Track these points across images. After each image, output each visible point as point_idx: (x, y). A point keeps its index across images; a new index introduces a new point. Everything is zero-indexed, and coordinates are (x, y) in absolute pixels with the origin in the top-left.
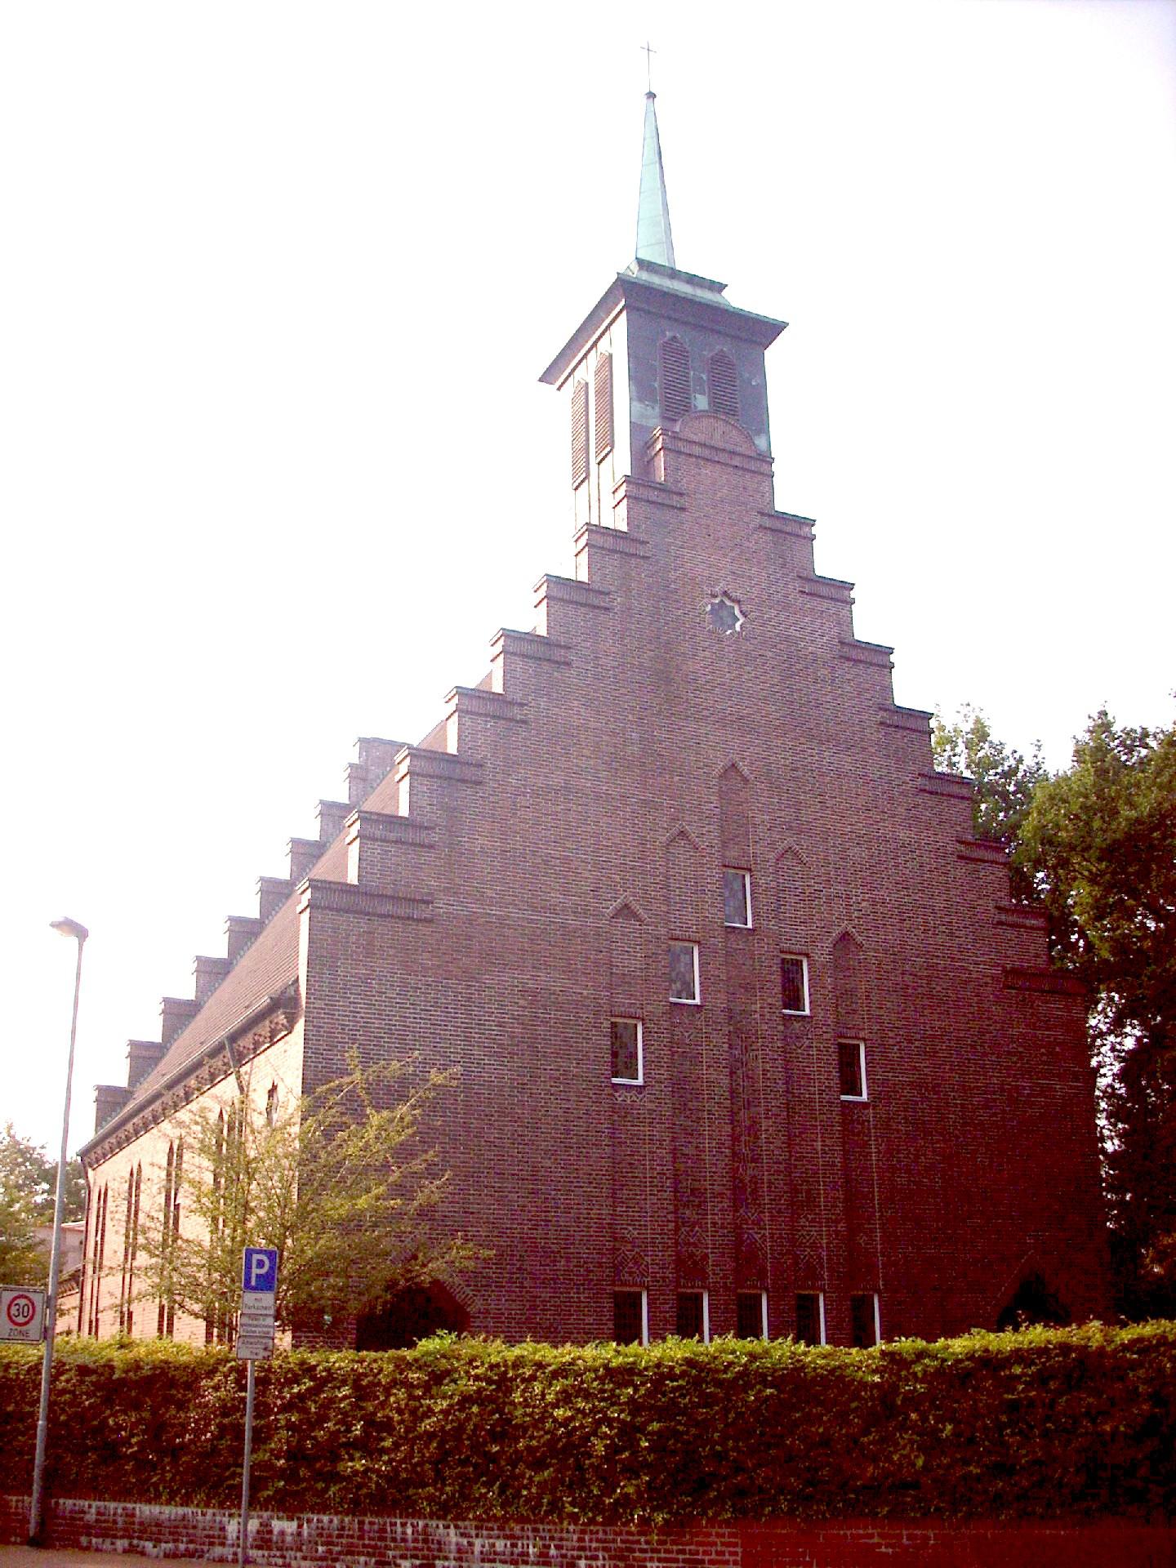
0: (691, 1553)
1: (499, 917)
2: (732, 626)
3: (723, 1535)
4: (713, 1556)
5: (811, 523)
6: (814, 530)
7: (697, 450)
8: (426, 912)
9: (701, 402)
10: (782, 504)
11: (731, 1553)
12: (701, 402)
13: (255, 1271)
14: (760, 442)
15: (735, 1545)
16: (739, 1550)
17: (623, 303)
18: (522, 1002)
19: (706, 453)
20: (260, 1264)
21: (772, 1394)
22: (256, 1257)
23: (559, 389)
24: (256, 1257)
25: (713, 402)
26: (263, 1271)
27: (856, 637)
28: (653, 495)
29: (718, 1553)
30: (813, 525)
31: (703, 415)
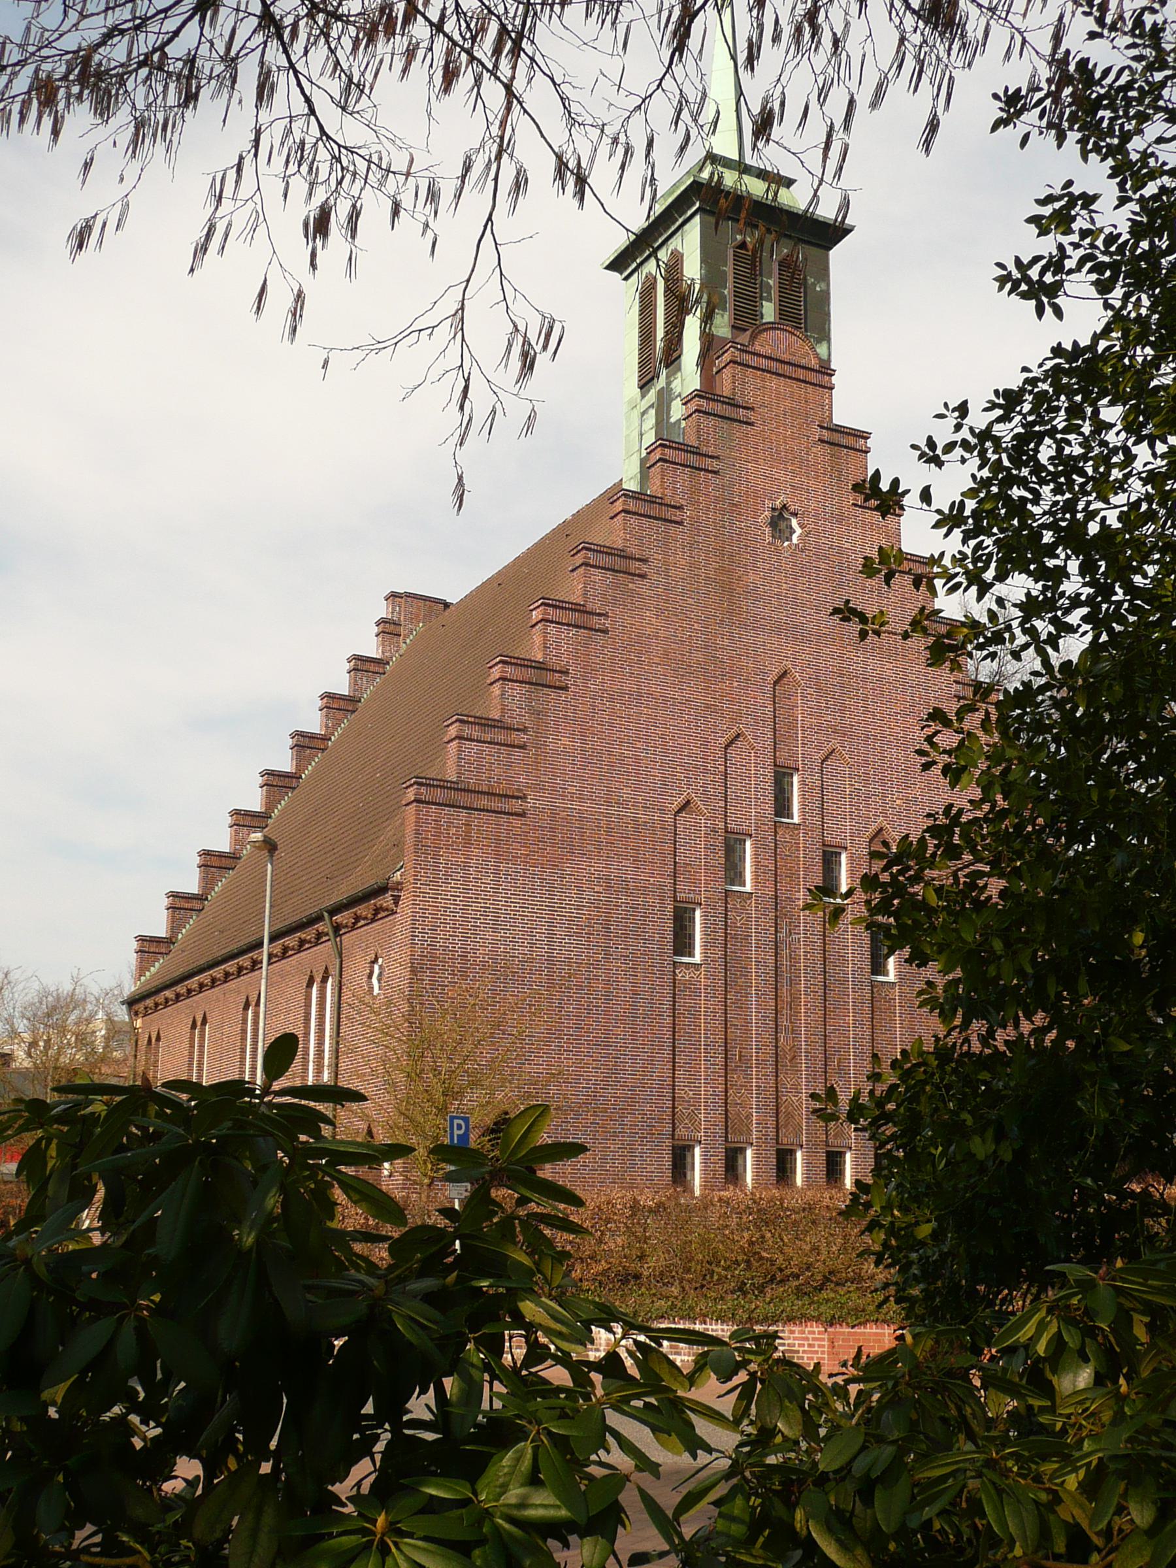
0: (789, 1345)
1: (580, 812)
2: (789, 539)
3: (814, 1333)
4: (806, 1348)
5: (865, 436)
6: (869, 443)
7: (764, 363)
8: (516, 805)
9: (769, 311)
10: (840, 418)
11: (819, 1346)
12: (769, 311)
13: (456, 1132)
14: (822, 350)
15: (823, 1340)
16: (826, 1343)
17: (698, 205)
18: (597, 889)
19: (773, 365)
20: (459, 1127)
21: (1169, 1328)
22: (456, 1122)
23: (626, 279)
24: (456, 1122)
25: (782, 313)
26: (461, 1132)
27: (835, 422)
28: (719, 408)
29: (810, 1345)
30: (832, 375)
31: (771, 327)
